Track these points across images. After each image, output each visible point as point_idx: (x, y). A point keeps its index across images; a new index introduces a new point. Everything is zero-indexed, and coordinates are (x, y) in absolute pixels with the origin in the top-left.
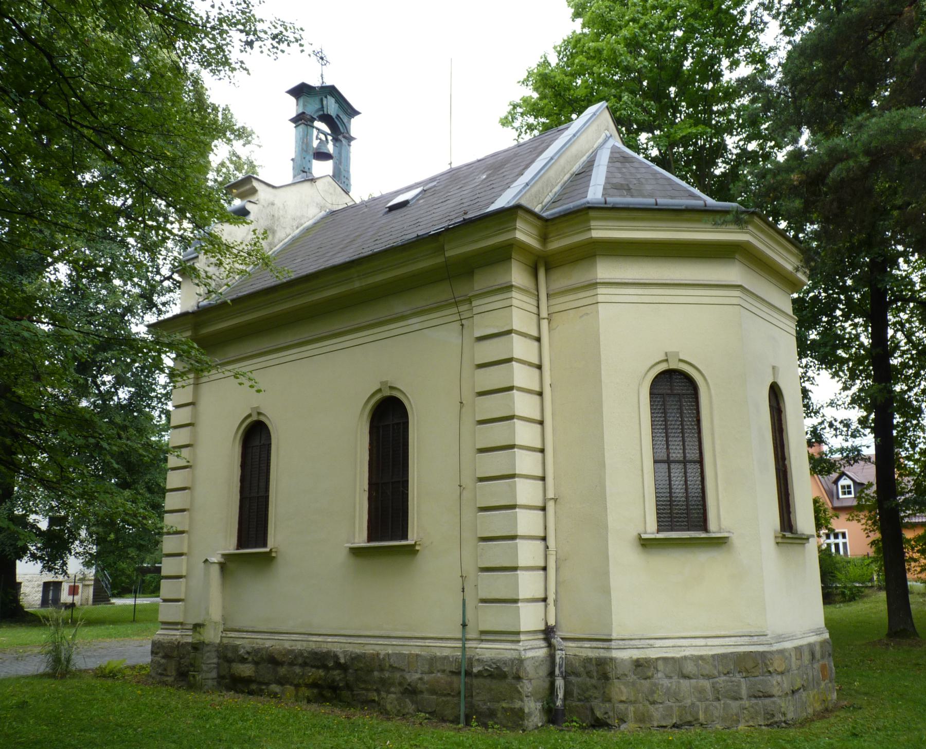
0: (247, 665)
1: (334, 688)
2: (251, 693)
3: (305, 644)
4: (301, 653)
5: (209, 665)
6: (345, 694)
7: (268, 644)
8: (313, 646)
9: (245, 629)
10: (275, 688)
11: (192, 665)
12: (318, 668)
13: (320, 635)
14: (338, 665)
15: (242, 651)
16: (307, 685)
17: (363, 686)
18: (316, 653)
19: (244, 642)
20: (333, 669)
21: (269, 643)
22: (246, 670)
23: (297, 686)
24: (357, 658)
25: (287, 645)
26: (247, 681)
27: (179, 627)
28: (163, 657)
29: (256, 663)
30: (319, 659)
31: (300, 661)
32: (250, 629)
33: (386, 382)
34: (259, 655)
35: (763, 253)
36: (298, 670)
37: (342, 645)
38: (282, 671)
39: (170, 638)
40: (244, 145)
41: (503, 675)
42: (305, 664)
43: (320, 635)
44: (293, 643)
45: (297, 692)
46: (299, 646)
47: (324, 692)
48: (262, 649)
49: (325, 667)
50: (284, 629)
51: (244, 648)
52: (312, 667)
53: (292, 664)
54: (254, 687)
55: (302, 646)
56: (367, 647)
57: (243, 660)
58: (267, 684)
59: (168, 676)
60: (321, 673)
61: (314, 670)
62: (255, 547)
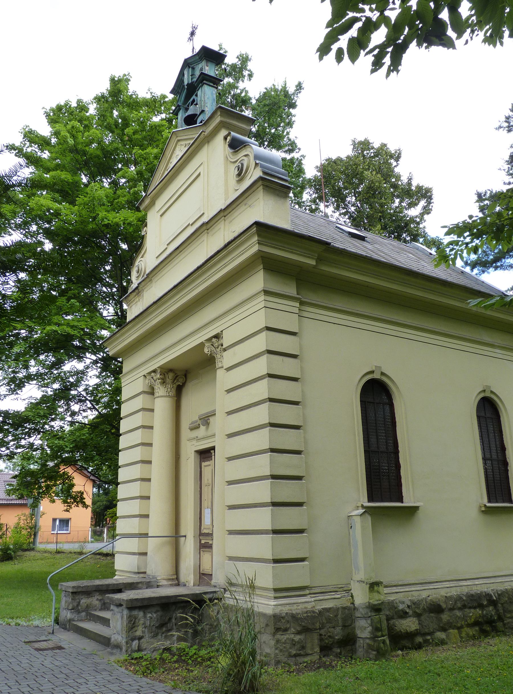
0: (409, 620)
1: (490, 622)
2: (419, 647)
3: (458, 589)
4: (459, 598)
5: (363, 630)
6: (499, 625)
7: (424, 595)
8: (465, 590)
9: (394, 583)
10: (440, 635)
11: (394, 625)
12: (475, 608)
13: (466, 580)
14: (493, 602)
15: (401, 607)
16: (469, 626)
17: (509, 615)
18: (472, 595)
19: (401, 597)
20: (487, 606)
21: (425, 594)
22: (410, 624)
23: (459, 628)
24: (501, 594)
25: (443, 593)
26: (410, 636)
27: (307, 592)
28: (299, 633)
29: (418, 616)
30: (476, 601)
31: (459, 605)
32: (400, 583)
33: (490, 387)
34: (421, 606)
35: (162, 320)
36: (458, 613)
37: (488, 585)
38: (445, 617)
39: (301, 606)
40: (243, 81)
41: (347, 615)
42: (464, 606)
43: (466, 580)
44: (448, 590)
45: (460, 633)
46: (454, 592)
47: (484, 627)
48: (422, 600)
49: (481, 606)
50: (433, 578)
51: (403, 603)
52: (470, 608)
53: (451, 609)
54: (419, 639)
55: (413, 596)
56: (506, 584)
57: (404, 615)
58: (431, 634)
59: (307, 655)
60: (479, 611)
61: (472, 610)
62: (382, 501)
